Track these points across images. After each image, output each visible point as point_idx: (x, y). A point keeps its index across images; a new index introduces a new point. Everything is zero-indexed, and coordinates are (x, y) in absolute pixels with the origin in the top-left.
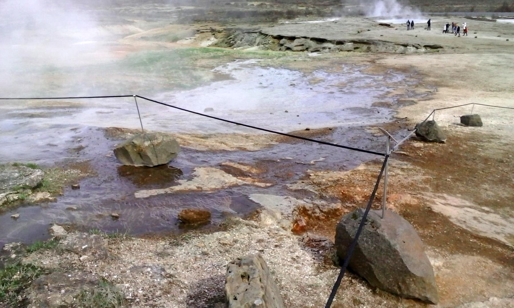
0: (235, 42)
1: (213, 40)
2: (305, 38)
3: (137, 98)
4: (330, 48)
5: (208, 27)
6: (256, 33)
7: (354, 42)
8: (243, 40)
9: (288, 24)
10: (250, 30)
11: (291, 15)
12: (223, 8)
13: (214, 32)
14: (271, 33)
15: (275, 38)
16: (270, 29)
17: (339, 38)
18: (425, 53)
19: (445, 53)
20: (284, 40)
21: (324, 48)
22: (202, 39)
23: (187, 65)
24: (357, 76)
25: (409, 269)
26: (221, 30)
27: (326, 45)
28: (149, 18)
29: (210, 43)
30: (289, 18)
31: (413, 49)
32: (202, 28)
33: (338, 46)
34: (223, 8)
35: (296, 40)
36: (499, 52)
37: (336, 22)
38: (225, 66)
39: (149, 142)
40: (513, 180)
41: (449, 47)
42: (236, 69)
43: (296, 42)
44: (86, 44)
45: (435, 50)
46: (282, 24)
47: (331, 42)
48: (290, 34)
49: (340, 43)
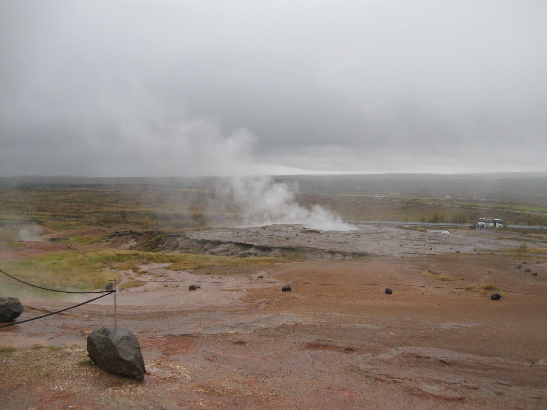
6: (179, 236)
48: (217, 239)
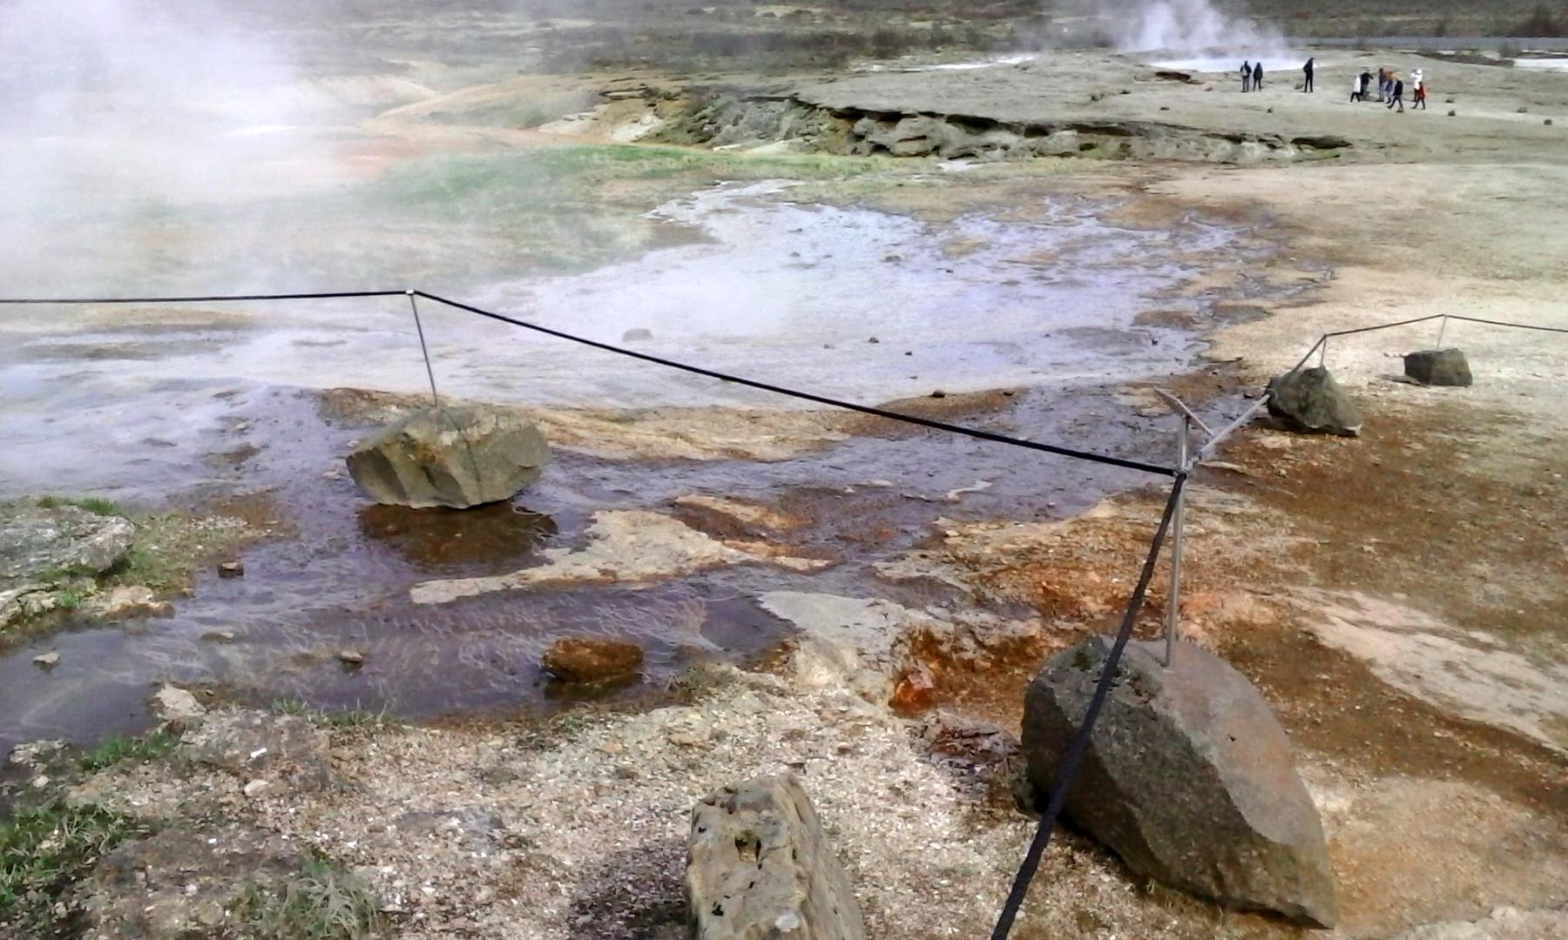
0: (718, 129)
1: (650, 122)
2: (931, 115)
3: (419, 300)
4: (1005, 148)
5: (635, 84)
6: (781, 99)
7: (1081, 128)
8: (741, 122)
9: (880, 72)
10: (763, 90)
11: (887, 46)
12: (680, 24)
13: (653, 99)
14: (826, 102)
15: (838, 115)
16: (825, 88)
17: (1036, 116)
18: (1298, 161)
19: (1356, 161)
20: (865, 121)
21: (988, 147)
22: (618, 119)
23: (570, 199)
24: (1088, 231)
25: (1248, 820)
26: (674, 91)
27: (993, 137)
28: (454, 55)
29: (640, 130)
30: (881, 55)
31: (1259, 150)
32: (617, 85)
33: (1032, 141)
34: (680, 24)
35: (903, 123)
36: (1523, 159)
37: (1024, 68)
38: (686, 202)
39: (455, 434)
40: (1567, 549)
41: (1369, 143)
42: (719, 211)
43: (903, 129)
44: (261, 134)
45: (1327, 152)
46: (861, 74)
47: (1008, 127)
48: (885, 105)
49: (1038, 130)
